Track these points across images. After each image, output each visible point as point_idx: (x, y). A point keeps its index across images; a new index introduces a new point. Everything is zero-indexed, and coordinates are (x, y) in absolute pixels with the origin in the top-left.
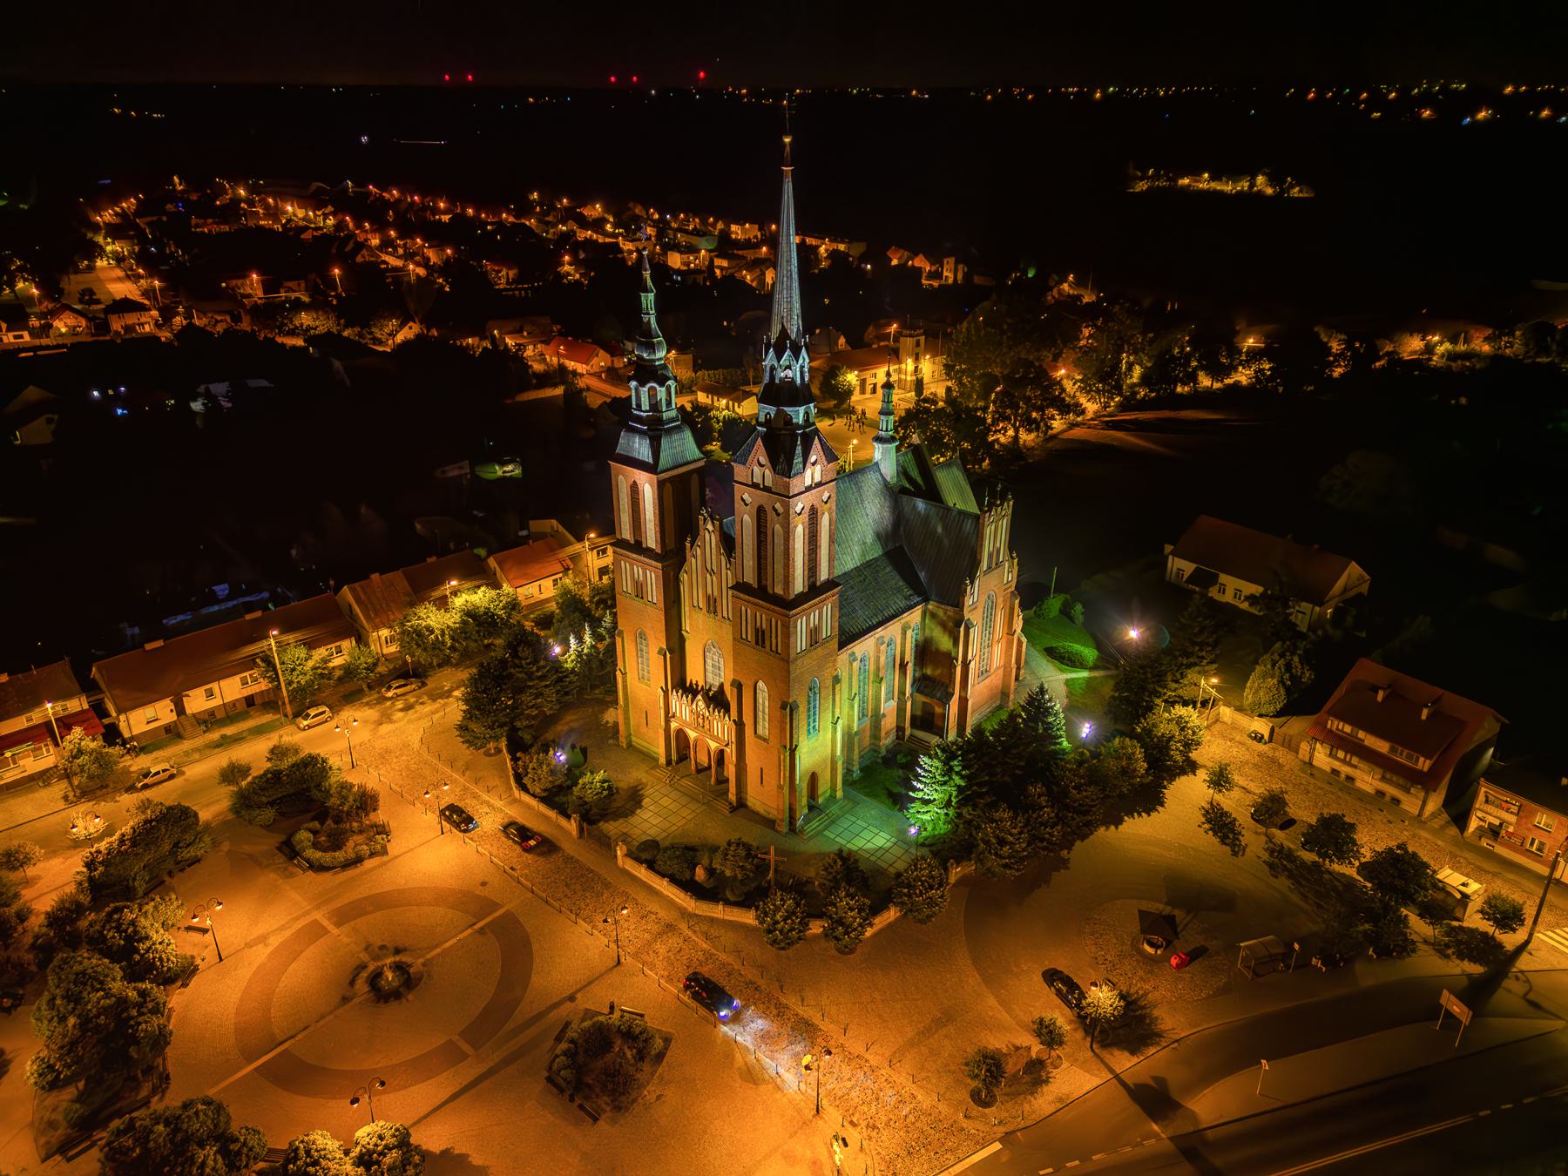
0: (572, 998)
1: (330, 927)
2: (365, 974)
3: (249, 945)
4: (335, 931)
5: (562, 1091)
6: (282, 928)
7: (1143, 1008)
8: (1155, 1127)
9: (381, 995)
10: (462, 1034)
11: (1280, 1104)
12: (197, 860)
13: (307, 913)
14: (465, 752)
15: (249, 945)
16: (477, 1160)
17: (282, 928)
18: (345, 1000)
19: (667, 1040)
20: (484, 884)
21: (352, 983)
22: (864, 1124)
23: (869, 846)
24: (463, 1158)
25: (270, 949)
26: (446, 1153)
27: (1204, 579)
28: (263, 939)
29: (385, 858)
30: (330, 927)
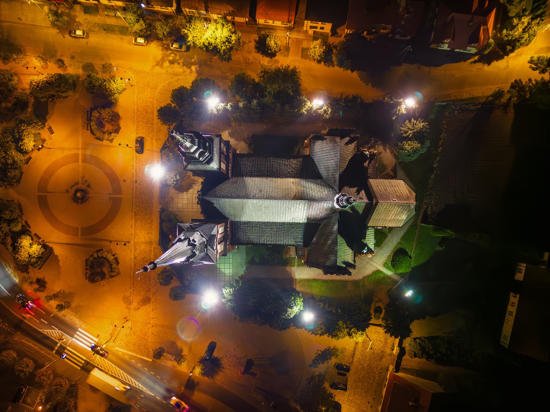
0: (111, 242)
1: (80, 161)
2: (76, 187)
3: (60, 149)
4: (80, 163)
5: (86, 266)
6: (70, 149)
7: (219, 370)
8: (183, 389)
9: (75, 199)
10: (82, 228)
11: (311, 278)
12: (66, 97)
13: (78, 149)
14: (157, 121)
15: (60, 149)
16: (61, 264)
17: (70, 149)
18: (67, 191)
19: (118, 274)
20: (124, 181)
21: (72, 187)
22: (133, 331)
23: (223, 270)
24: (58, 261)
25: (63, 155)
26: (57, 256)
27: (517, 287)
28: (62, 149)
29: (110, 144)
30: (80, 161)
